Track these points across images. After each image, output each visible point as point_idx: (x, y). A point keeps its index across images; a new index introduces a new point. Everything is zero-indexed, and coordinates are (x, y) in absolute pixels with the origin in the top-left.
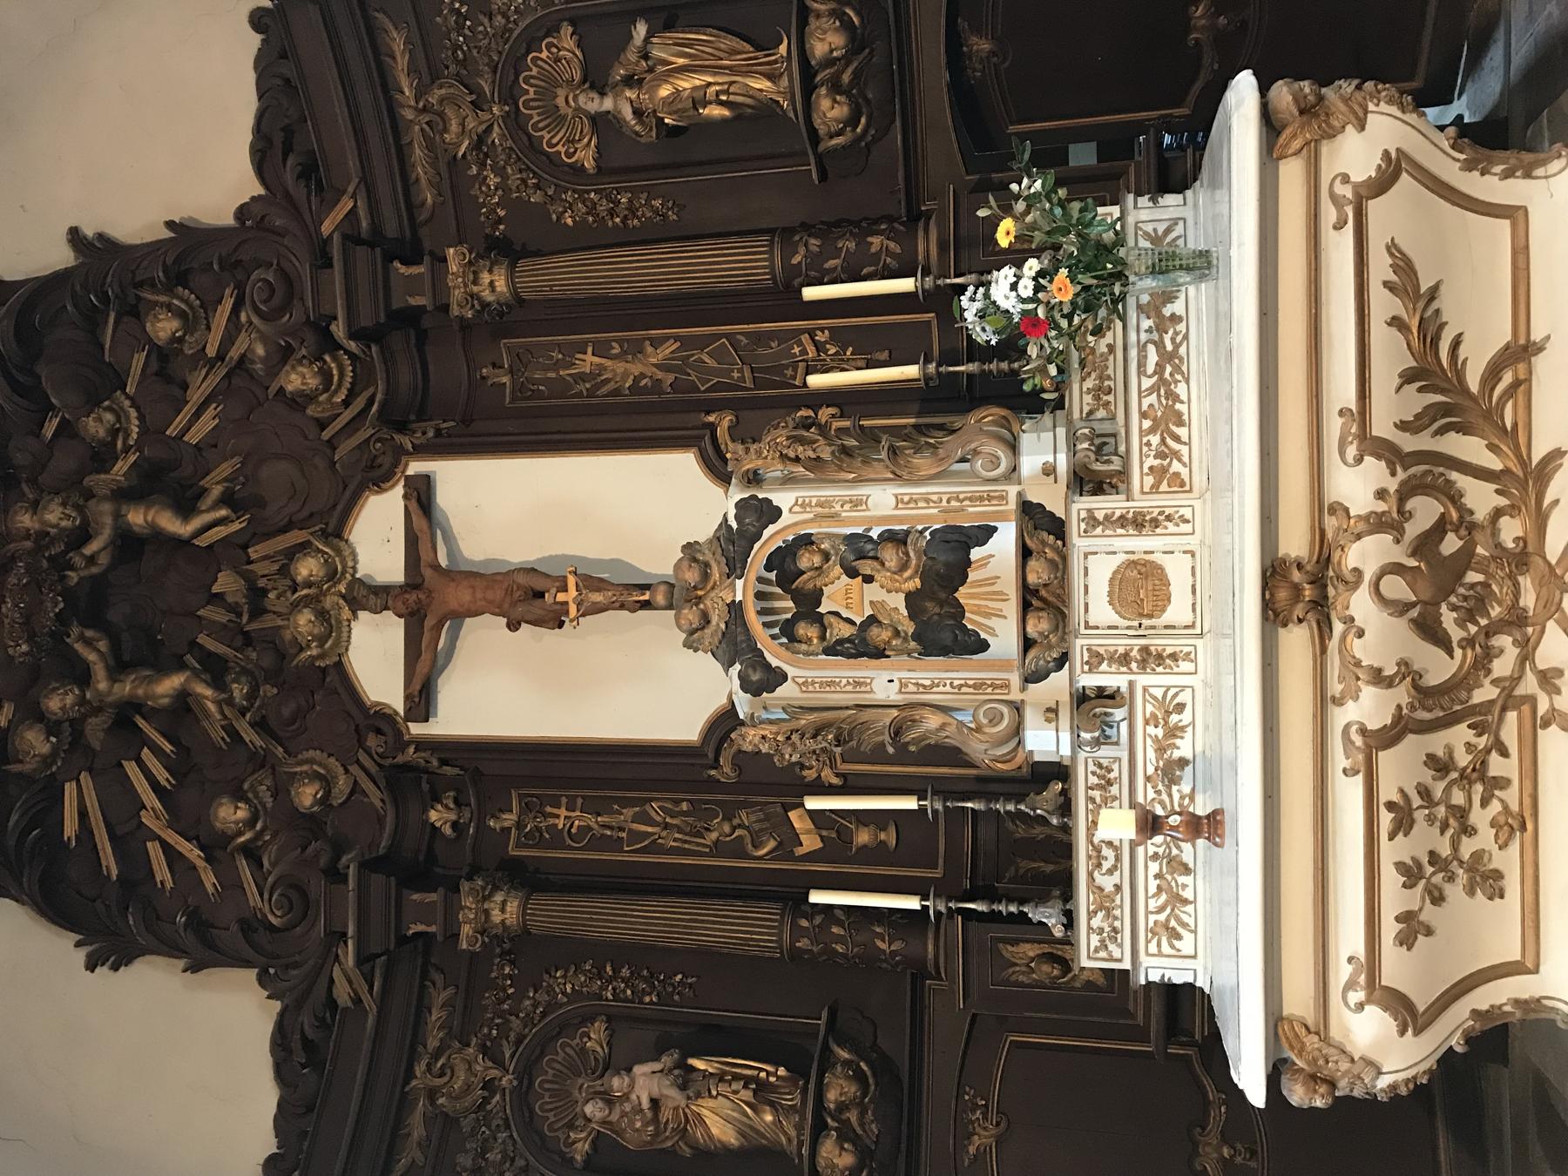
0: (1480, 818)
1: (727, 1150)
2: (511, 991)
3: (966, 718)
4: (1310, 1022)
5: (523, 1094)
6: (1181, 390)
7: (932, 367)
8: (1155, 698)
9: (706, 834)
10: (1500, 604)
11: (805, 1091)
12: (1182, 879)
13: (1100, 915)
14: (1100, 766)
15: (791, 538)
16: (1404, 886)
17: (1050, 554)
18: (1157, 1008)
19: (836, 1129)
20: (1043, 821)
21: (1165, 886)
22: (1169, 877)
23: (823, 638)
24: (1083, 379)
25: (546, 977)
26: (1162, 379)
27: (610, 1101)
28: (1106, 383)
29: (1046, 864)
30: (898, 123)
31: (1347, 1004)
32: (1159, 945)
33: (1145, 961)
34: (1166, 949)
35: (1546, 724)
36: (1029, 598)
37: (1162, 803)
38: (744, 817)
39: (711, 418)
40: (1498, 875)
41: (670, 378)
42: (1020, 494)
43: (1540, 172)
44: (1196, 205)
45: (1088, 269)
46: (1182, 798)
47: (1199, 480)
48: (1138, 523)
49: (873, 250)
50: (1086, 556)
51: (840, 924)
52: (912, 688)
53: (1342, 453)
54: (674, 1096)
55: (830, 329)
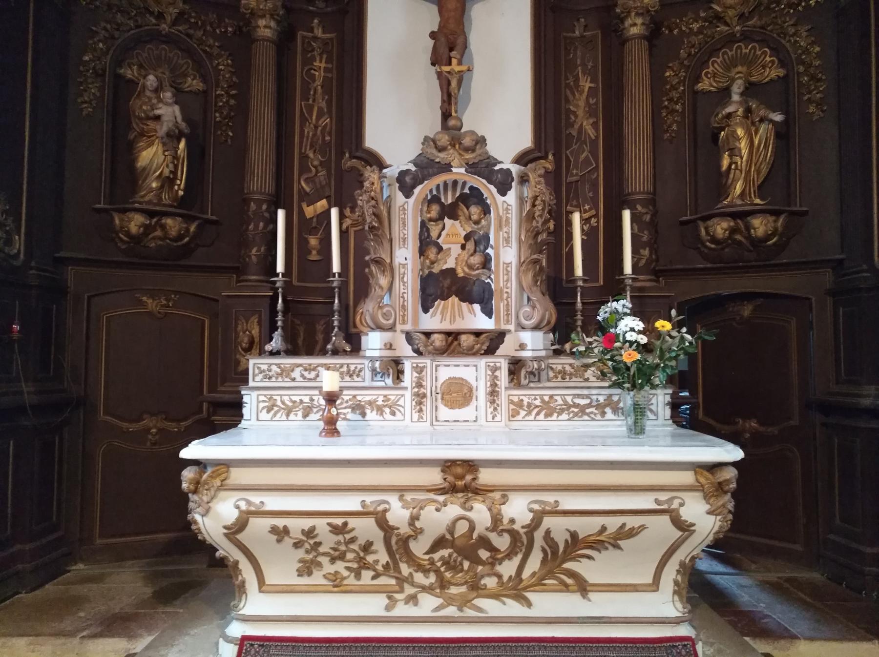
0: (340, 566)
1: (133, 161)
2: (218, 31)
3: (386, 300)
4: (227, 482)
5: (156, 37)
6: (565, 416)
7: (580, 283)
8: (398, 401)
9: (312, 151)
10: (452, 577)
11: (171, 206)
12: (300, 414)
13: (278, 370)
14: (360, 371)
15: (488, 202)
16: (303, 530)
17: (477, 347)
18: (226, 397)
19: (150, 223)
20: (328, 340)
21: (296, 404)
22: (301, 407)
23: (431, 220)
24: (571, 365)
25: (227, 53)
26: (571, 406)
27: (157, 91)
28: (568, 377)
29: (305, 342)
30: (709, 265)
31: (238, 500)
32: (264, 401)
33: (254, 394)
34: (262, 405)
35: (389, 598)
36: (452, 336)
37: (341, 403)
38: (323, 173)
39: (550, 157)
40: (310, 574)
41: (574, 133)
42: (509, 331)
43: (676, 598)
44: (664, 425)
45: (639, 369)
46: (344, 414)
47: (515, 425)
48: (493, 393)
49: (642, 251)
50: (476, 366)
51: (265, 227)
52: (402, 270)
53: (535, 502)
54: (163, 129)
55: (598, 226)
